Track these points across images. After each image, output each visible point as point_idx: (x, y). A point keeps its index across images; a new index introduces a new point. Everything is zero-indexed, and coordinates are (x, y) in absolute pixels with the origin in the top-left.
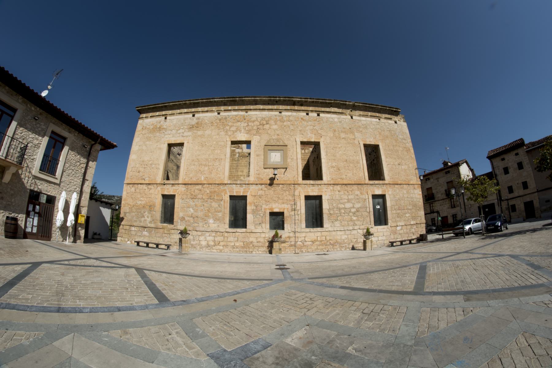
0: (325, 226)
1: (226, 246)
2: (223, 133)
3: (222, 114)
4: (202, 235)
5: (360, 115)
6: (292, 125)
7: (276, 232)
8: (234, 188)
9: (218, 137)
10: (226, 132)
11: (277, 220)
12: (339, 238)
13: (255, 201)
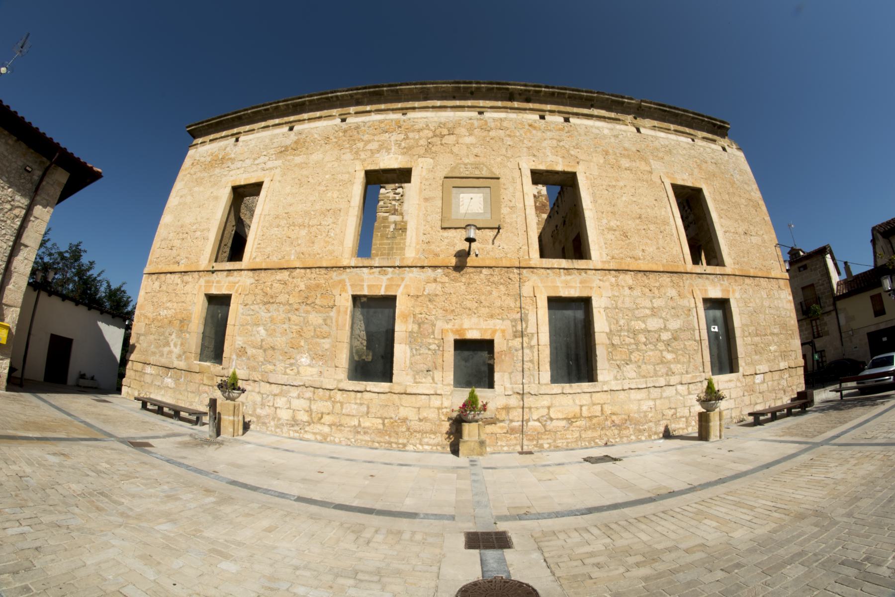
0: (600, 377)
1: (339, 426)
2: (348, 156)
3: (350, 120)
4: (280, 394)
5: (654, 128)
6: (509, 136)
7: (472, 393)
8: (365, 276)
9: (336, 164)
10: (357, 153)
11: (476, 360)
12: (634, 407)
13: (417, 310)
